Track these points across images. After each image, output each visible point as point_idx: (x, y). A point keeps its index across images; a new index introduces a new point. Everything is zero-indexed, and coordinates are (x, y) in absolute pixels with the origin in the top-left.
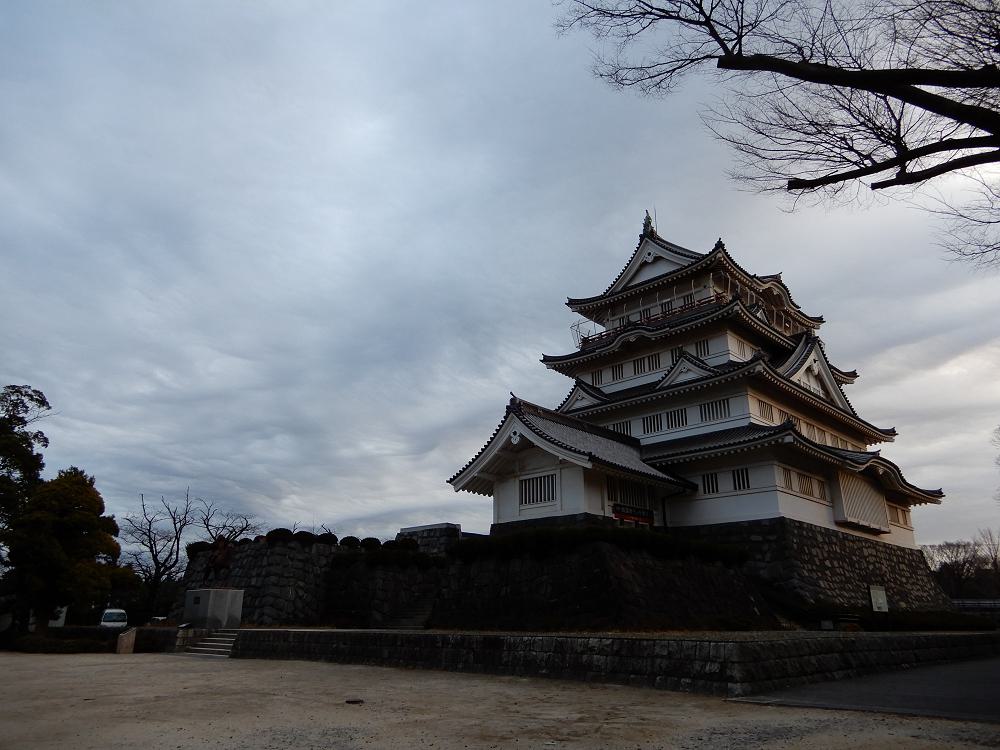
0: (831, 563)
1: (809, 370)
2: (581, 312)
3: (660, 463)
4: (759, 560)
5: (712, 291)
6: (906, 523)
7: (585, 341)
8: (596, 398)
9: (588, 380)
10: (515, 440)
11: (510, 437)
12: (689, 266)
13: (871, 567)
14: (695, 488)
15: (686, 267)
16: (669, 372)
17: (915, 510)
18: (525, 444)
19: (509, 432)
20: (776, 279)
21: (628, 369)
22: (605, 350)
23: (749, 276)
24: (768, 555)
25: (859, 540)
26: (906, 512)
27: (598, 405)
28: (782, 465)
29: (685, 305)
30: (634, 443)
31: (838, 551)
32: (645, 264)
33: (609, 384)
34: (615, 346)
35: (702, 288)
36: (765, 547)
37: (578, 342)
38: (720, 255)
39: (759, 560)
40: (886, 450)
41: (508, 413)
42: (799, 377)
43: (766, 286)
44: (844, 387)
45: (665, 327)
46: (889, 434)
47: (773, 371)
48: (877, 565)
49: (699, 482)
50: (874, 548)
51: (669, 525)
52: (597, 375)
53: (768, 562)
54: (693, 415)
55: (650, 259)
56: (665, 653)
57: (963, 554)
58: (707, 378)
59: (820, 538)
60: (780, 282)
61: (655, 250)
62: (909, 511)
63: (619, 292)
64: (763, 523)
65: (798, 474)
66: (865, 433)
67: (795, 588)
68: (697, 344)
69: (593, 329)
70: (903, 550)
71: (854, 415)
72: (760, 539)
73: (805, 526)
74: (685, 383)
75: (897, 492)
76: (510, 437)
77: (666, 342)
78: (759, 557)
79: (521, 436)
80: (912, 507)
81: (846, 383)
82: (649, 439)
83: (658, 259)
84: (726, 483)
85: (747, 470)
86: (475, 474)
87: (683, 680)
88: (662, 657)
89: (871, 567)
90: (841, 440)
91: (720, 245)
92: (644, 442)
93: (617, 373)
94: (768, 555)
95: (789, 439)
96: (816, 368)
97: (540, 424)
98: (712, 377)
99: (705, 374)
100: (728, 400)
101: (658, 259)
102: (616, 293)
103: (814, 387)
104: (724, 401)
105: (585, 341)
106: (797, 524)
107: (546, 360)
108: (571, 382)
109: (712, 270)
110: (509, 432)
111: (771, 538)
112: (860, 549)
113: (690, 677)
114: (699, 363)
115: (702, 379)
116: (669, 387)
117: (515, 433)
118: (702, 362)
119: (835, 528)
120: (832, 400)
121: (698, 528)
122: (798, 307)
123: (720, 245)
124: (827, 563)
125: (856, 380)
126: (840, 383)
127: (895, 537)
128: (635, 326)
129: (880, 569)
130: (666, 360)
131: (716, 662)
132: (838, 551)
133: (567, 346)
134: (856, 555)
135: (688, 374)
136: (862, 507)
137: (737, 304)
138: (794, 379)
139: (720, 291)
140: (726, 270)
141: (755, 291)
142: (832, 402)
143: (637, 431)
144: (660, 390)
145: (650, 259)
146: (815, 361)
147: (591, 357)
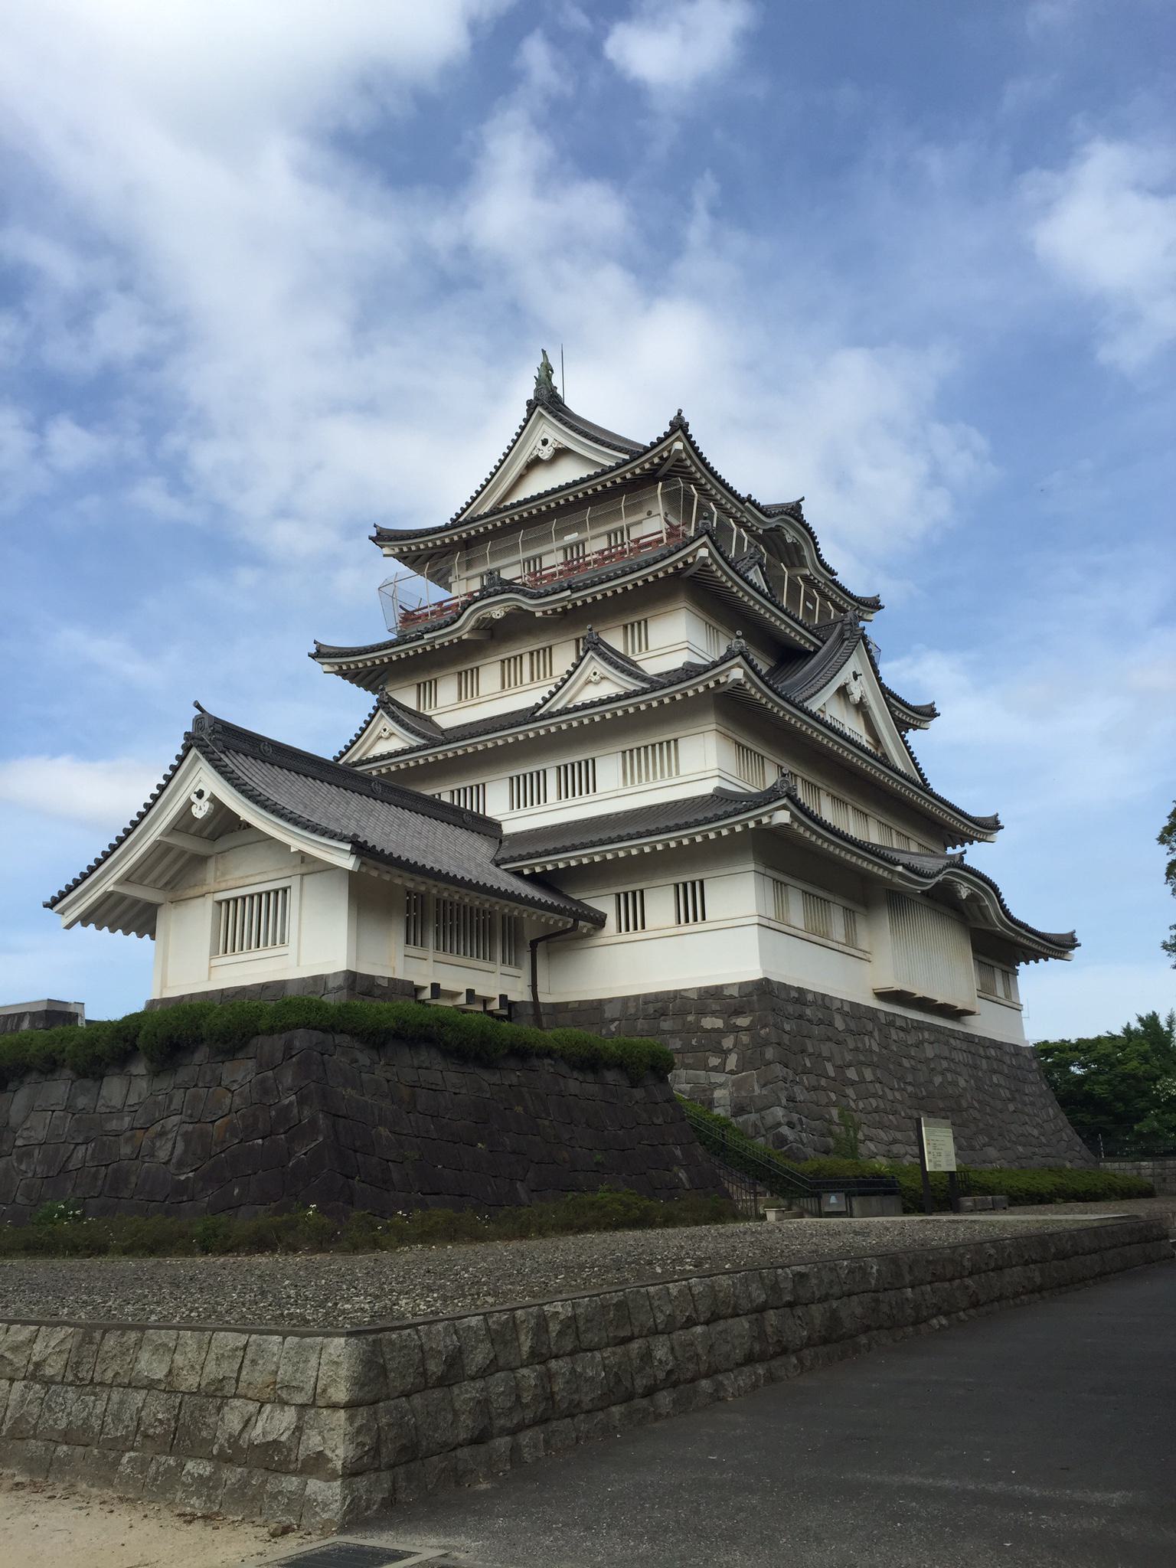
0: (860, 1074)
1: (843, 692)
2: (402, 558)
3: (531, 867)
4: (715, 1069)
5: (651, 523)
6: (1008, 996)
7: (408, 617)
8: (418, 734)
9: (408, 698)
10: (201, 809)
11: (190, 804)
12: (618, 466)
13: (938, 1080)
14: (599, 921)
15: (612, 469)
16: (559, 688)
17: (1028, 973)
18: (224, 824)
19: (186, 792)
20: (793, 511)
21: (490, 677)
22: (443, 638)
23: (737, 497)
24: (732, 1061)
25: (920, 1026)
26: (1010, 973)
27: (419, 749)
28: (769, 872)
29: (610, 549)
30: (488, 828)
31: (875, 1048)
32: (535, 463)
33: (451, 706)
34: (464, 628)
35: (644, 515)
36: (728, 1042)
37: (394, 619)
38: (679, 446)
39: (715, 1069)
40: (977, 855)
41: (187, 749)
42: (825, 703)
43: (772, 522)
44: (912, 736)
45: (563, 590)
46: (989, 826)
47: (770, 687)
48: (949, 1077)
49: (606, 905)
50: (947, 1043)
51: (542, 999)
52: (427, 689)
53: (732, 1072)
54: (609, 770)
55: (546, 453)
56: (160, 1373)
57: (895, 1037)
58: (635, 694)
59: (839, 1024)
60: (799, 519)
61: (551, 433)
62: (1016, 973)
63: (486, 515)
64: (726, 992)
65: (845, 909)
66: (948, 826)
67: (779, 1124)
68: (625, 627)
69: (423, 592)
70: (999, 1046)
71: (924, 786)
72: (719, 1023)
73: (810, 997)
74: (593, 704)
75: (1005, 946)
76: (190, 804)
77: (567, 620)
78: (714, 1061)
79: (213, 799)
80: (1022, 967)
81: (915, 728)
82: (516, 821)
83: (561, 453)
84: (660, 906)
85: (702, 883)
86: (108, 885)
87: (190, 1465)
88: (151, 1385)
89: (938, 1080)
90: (898, 833)
91: (679, 426)
92: (508, 829)
93: (468, 681)
94: (732, 1061)
95: (783, 817)
96: (856, 691)
97: (290, 789)
98: (644, 692)
99: (632, 685)
100: (676, 740)
101: (561, 453)
102: (480, 518)
103: (853, 726)
104: (532, 654)
105: (408, 617)
106: (794, 994)
107: (321, 653)
108: (370, 699)
109: (665, 478)
110: (186, 792)
111: (743, 1021)
112: (919, 1044)
113: (210, 1458)
114: (624, 665)
115: (628, 696)
116: (566, 711)
117: (200, 794)
118: (634, 664)
119: (875, 1004)
120: (884, 755)
121: (599, 1005)
122: (833, 573)
123: (679, 426)
124: (852, 1074)
125: (934, 723)
126: (902, 726)
127: (988, 1023)
128: (508, 586)
129: (955, 1084)
130: (563, 658)
131: (284, 1403)
132: (875, 1048)
133: (374, 630)
134: (909, 1057)
135: (599, 685)
136: (923, 962)
137: (704, 545)
138: (814, 706)
139: (675, 522)
140: (690, 479)
141: (748, 530)
142: (884, 760)
143: (497, 802)
144: (543, 718)
145: (546, 453)
146: (856, 676)
147: (414, 649)
